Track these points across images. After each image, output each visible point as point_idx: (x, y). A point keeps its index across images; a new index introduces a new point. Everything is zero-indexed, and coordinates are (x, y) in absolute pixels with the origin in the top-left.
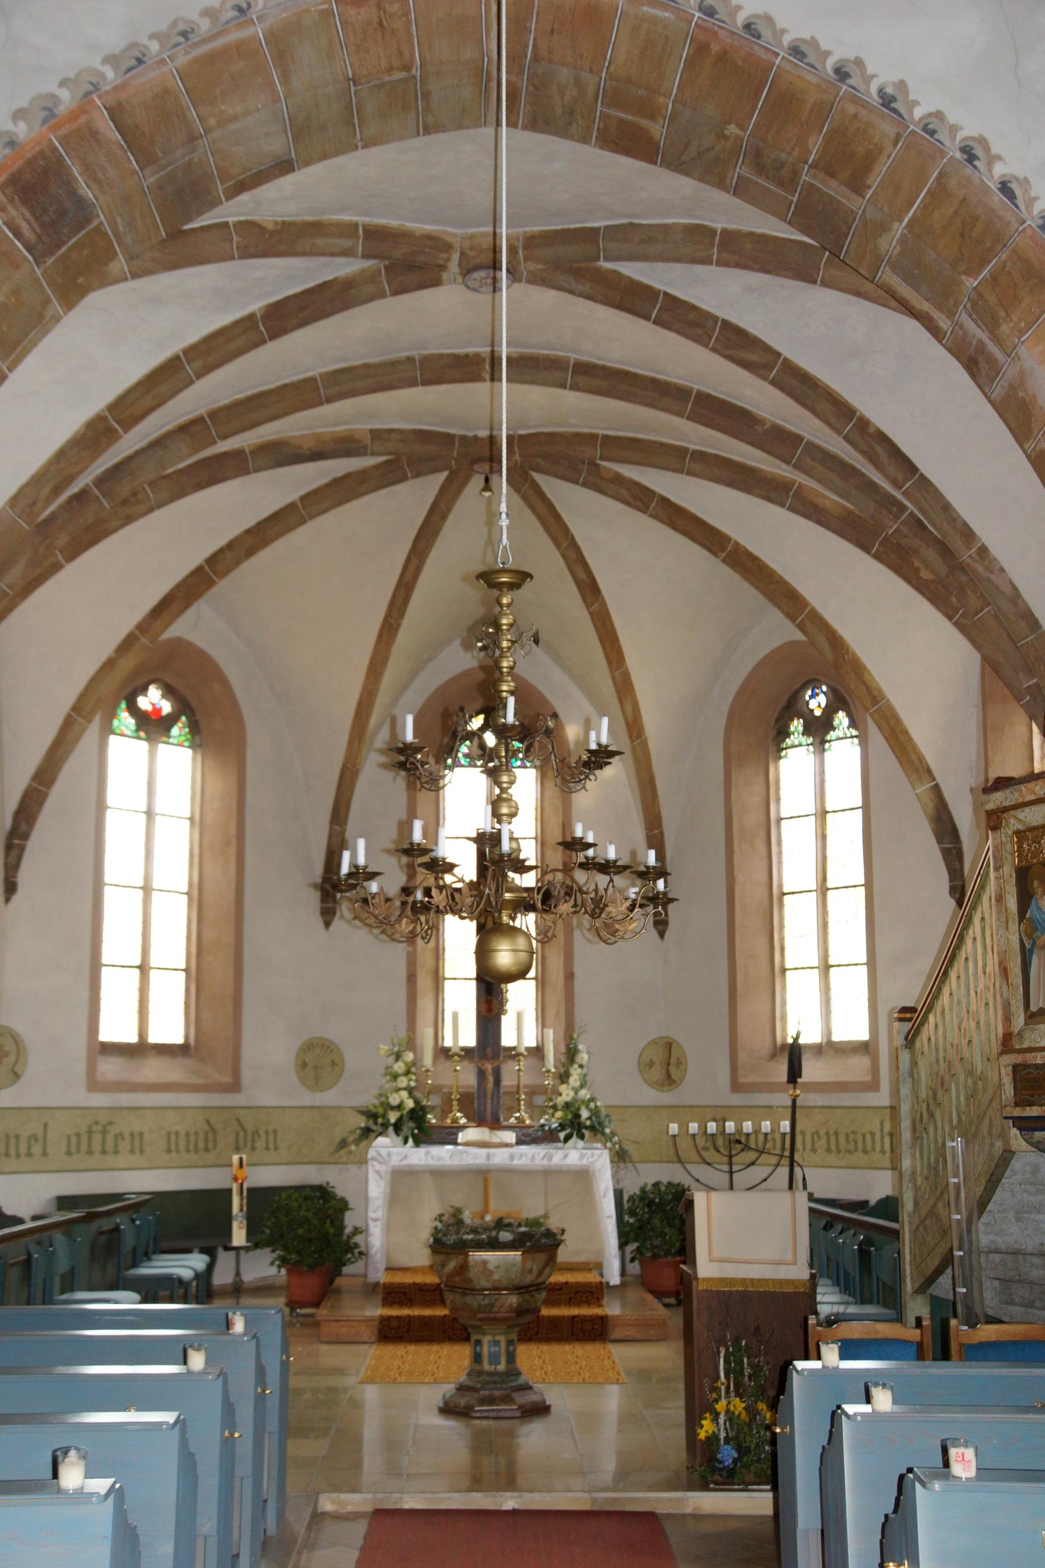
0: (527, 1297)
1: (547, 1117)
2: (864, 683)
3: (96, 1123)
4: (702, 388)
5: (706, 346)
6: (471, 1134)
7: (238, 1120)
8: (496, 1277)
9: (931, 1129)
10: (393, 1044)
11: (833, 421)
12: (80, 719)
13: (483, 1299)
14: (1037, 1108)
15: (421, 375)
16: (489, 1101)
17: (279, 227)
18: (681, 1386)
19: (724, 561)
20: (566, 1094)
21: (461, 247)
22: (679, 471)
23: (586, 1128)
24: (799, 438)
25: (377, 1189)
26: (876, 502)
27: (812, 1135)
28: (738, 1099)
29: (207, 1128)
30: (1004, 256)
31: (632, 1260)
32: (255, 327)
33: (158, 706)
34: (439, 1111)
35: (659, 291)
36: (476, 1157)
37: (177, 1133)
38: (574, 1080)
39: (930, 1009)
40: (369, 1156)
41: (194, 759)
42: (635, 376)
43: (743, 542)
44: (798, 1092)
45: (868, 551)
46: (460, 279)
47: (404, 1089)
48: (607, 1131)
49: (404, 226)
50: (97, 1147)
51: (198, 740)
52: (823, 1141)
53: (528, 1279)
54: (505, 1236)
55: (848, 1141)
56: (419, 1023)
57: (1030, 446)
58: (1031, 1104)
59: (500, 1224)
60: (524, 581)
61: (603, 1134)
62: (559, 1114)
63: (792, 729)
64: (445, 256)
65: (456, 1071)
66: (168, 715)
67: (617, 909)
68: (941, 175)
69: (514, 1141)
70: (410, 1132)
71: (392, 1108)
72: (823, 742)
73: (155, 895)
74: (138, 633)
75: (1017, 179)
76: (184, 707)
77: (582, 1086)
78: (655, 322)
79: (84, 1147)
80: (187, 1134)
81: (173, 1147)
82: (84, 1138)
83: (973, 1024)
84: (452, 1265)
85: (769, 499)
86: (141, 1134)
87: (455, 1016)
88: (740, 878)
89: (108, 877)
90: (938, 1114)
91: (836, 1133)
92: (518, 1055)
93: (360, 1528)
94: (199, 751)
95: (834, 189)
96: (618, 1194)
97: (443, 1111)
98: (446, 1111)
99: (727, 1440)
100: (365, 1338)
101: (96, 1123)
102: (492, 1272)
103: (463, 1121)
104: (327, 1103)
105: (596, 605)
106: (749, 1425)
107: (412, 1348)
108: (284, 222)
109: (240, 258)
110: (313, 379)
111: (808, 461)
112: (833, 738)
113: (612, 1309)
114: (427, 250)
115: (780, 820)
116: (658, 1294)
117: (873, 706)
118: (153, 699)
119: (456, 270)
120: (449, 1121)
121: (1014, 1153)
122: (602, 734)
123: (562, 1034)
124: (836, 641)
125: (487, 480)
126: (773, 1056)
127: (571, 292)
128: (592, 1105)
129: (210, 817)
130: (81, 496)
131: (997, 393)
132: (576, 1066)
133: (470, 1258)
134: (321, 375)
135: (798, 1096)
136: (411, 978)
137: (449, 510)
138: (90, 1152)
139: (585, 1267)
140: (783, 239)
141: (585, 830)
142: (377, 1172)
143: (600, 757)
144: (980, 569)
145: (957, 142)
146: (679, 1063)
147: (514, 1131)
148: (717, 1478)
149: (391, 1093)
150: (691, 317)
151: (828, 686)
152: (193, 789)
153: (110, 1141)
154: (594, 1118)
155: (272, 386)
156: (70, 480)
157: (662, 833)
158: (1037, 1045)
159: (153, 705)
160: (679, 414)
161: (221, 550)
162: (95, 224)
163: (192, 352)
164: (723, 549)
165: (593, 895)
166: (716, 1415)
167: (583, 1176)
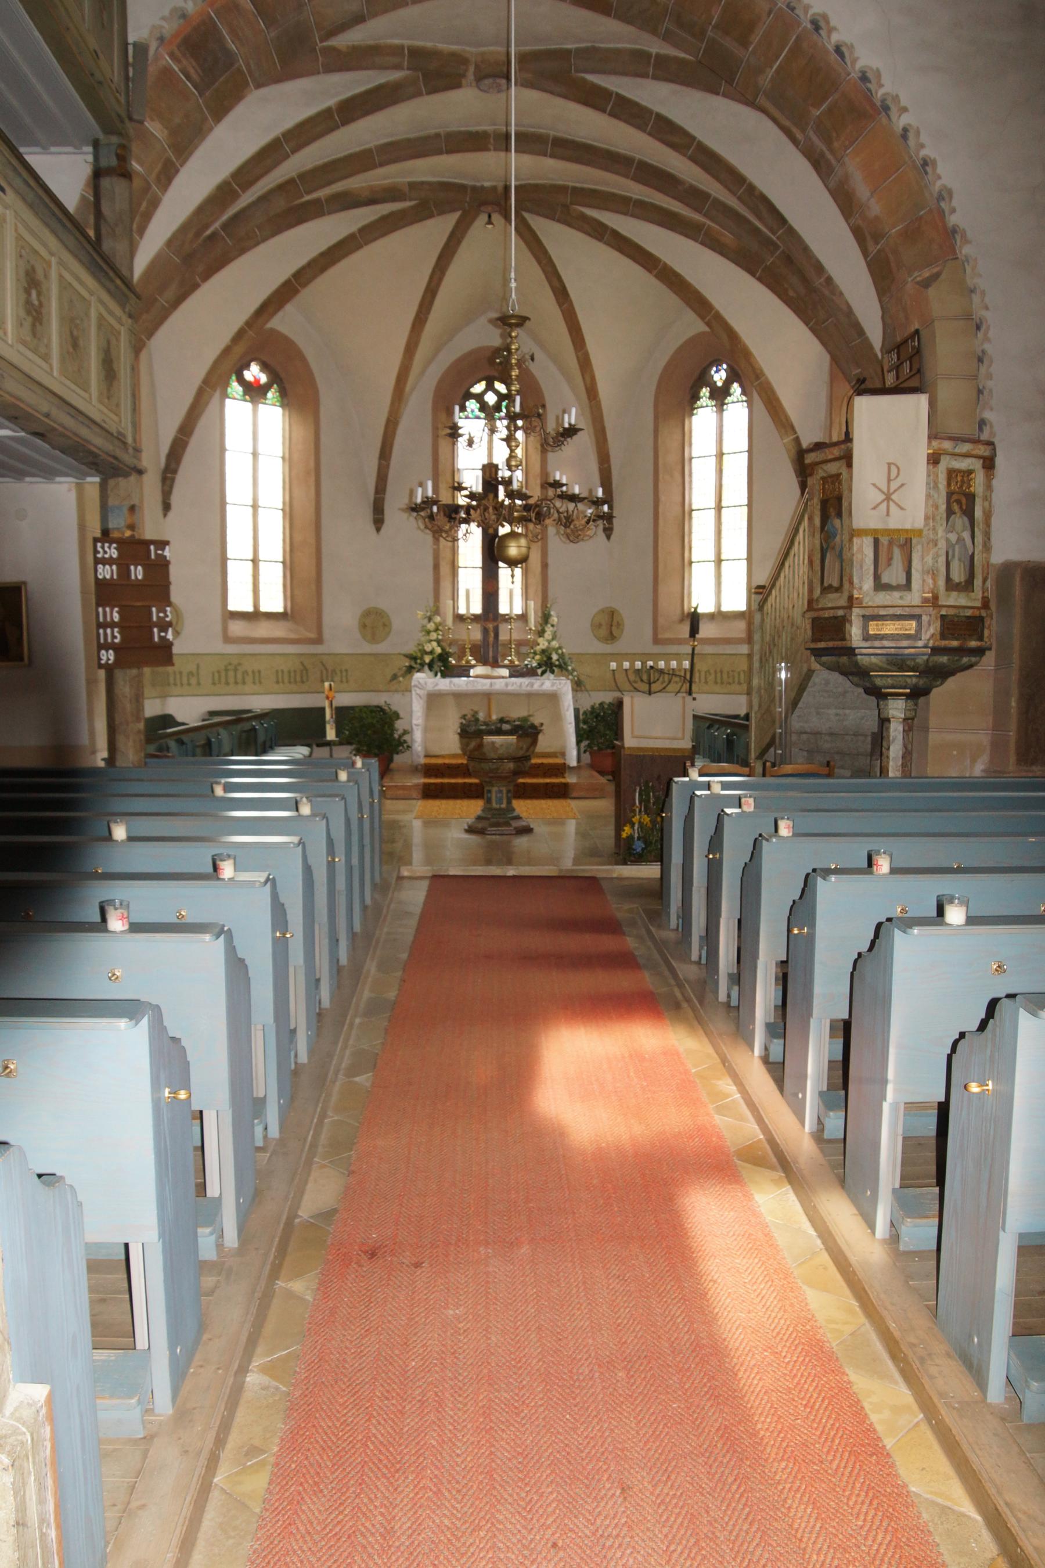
2: (751, 365)
4: (642, 158)
5: (644, 131)
6: (479, 670)
7: (322, 663)
8: (500, 751)
9: (771, 660)
15: (446, 146)
16: (491, 650)
18: (613, 820)
19: (656, 276)
20: (543, 644)
22: (625, 214)
23: (556, 666)
29: (302, 668)
30: (836, 96)
31: (585, 752)
34: (456, 656)
37: (283, 671)
38: (548, 635)
39: (773, 585)
40: (413, 684)
41: (284, 415)
43: (668, 262)
44: (696, 643)
46: (474, 84)
48: (570, 668)
50: (231, 680)
51: (286, 401)
53: (521, 753)
54: (506, 727)
55: (728, 677)
56: (442, 597)
57: (852, 221)
58: (821, 641)
59: (502, 721)
60: (525, 321)
61: (567, 670)
62: (538, 657)
63: (702, 394)
67: (580, 523)
68: (798, 38)
72: (723, 404)
75: (846, 44)
76: (276, 378)
77: (553, 639)
79: (223, 680)
80: (289, 672)
81: (280, 680)
82: (223, 674)
83: (796, 595)
84: (473, 744)
85: (687, 236)
86: (259, 672)
89: (229, 499)
90: (775, 651)
91: (721, 672)
92: (511, 618)
93: (425, 884)
95: (729, 43)
96: (577, 711)
97: (459, 657)
98: (461, 655)
99: (639, 838)
100: (414, 796)
101: (230, 664)
102: (497, 748)
105: (565, 305)
106: (652, 829)
107: (444, 802)
110: (370, 150)
113: (571, 779)
116: (602, 773)
118: (254, 373)
119: (472, 78)
120: (464, 662)
121: (814, 671)
122: (571, 418)
123: (539, 604)
124: (732, 335)
125: (490, 216)
126: (682, 620)
127: (552, 93)
130: (214, 236)
131: (832, 184)
132: (549, 626)
133: (485, 741)
134: (376, 147)
136: (436, 567)
137: (463, 238)
138: (227, 683)
139: (554, 755)
141: (561, 477)
143: (571, 431)
144: (827, 292)
145: (809, 16)
146: (619, 625)
148: (633, 859)
152: (284, 437)
153: (239, 676)
155: (341, 155)
156: (207, 226)
157: (609, 467)
159: (255, 377)
162: (236, 65)
163: (288, 135)
165: (565, 514)
166: (633, 825)
167: (553, 698)
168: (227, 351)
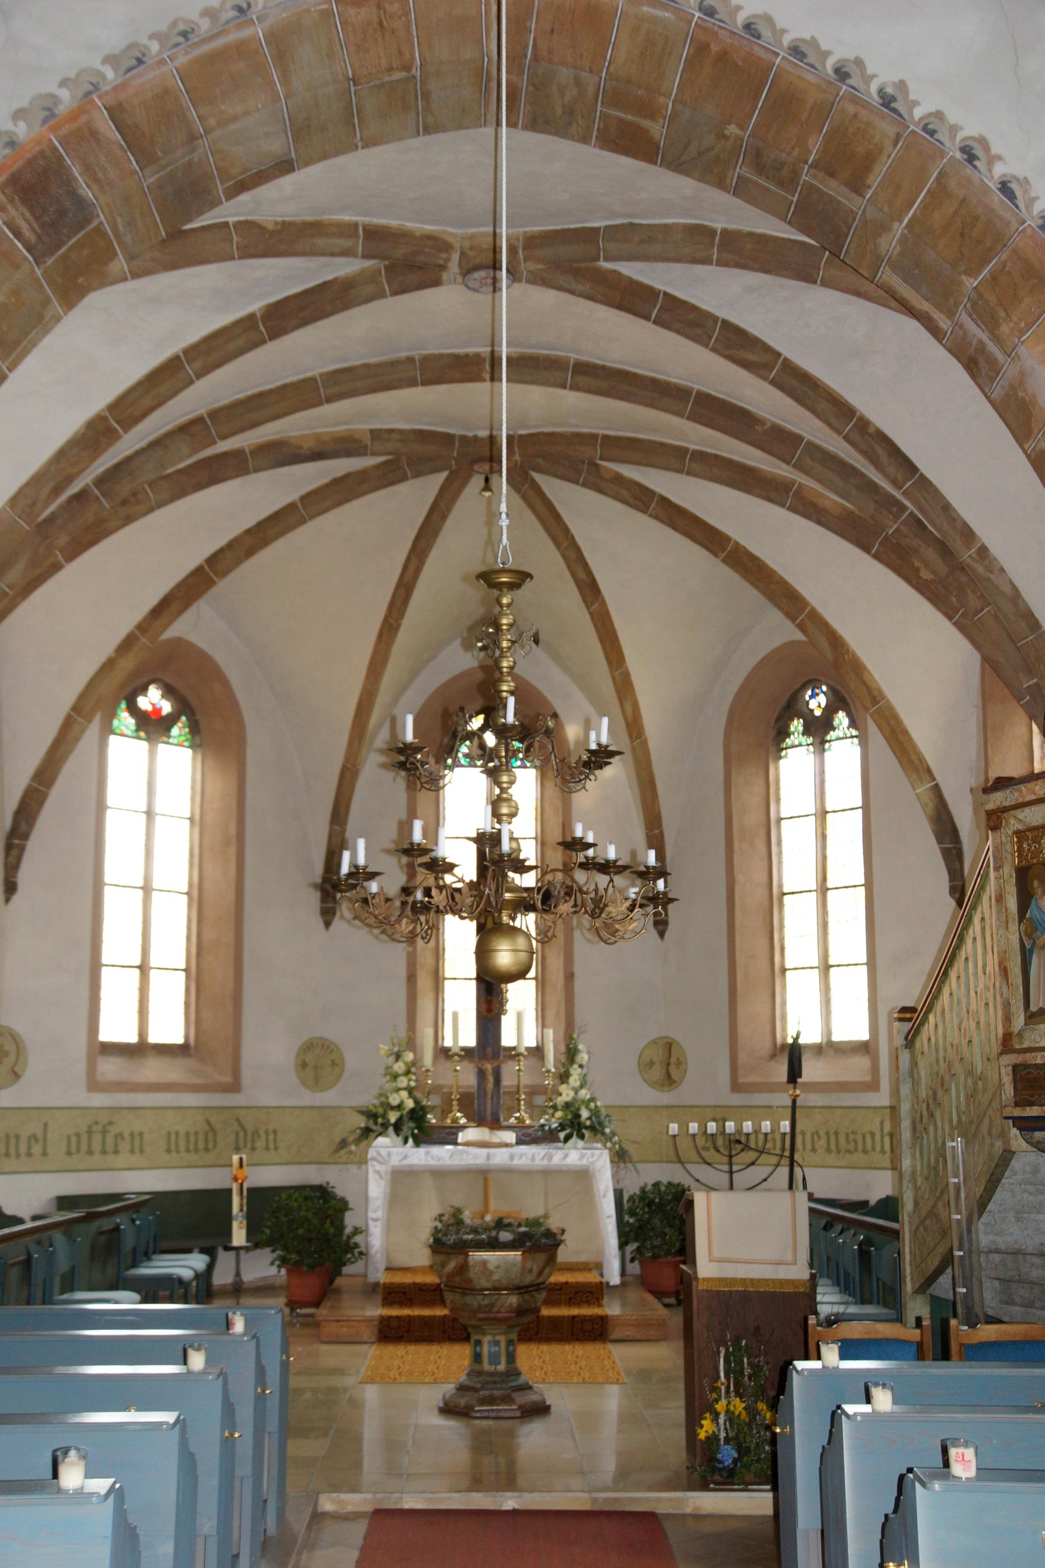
0: (527, 1297)
1: (547, 1117)
2: (864, 683)
3: (96, 1123)
4: (702, 388)
5: (706, 346)
6: (471, 1134)
7: (238, 1120)
8: (496, 1277)
9: (931, 1129)
10: (393, 1044)
11: (833, 421)
12: (80, 719)
13: (483, 1299)
14: (1037, 1108)
15: (421, 375)
16: (489, 1101)
17: (279, 227)
18: (681, 1386)
19: (724, 561)
20: (566, 1094)
21: (461, 247)
22: (679, 471)
23: (586, 1128)
24: (799, 438)
25: (377, 1189)
26: (876, 502)
27: (812, 1135)
28: (738, 1099)
29: (207, 1128)
30: (1004, 256)
31: (632, 1260)
32: (255, 327)
33: (158, 706)
34: (439, 1111)
35: (659, 291)
36: (476, 1157)
37: (177, 1133)
38: (574, 1080)
39: (930, 1009)
40: (369, 1156)
41: (194, 759)
42: (635, 376)
43: (743, 542)
44: (798, 1092)
45: (868, 551)
46: (460, 279)
47: (404, 1089)
48: (607, 1131)
49: (404, 226)
50: (97, 1147)
51: (198, 740)
52: (823, 1141)
53: (528, 1279)
54: (505, 1236)
55: (848, 1141)
56: (419, 1023)
57: (1030, 446)
58: (1031, 1104)
59: (500, 1224)
60: (524, 581)
61: (603, 1134)
62: (559, 1114)
63: (792, 729)
64: (445, 256)
65: (456, 1071)
66: (168, 715)
67: (617, 909)
68: (941, 175)
69: (514, 1141)
70: (410, 1132)
71: (392, 1108)
72: (823, 742)
73: (155, 895)
74: (138, 633)
75: (1017, 179)
76: (184, 707)
77: (582, 1086)
78: (655, 322)
79: (84, 1147)
80: (187, 1134)
81: (173, 1147)
82: (84, 1138)
83: (973, 1024)
84: (452, 1265)
85: (769, 499)
86: (141, 1134)
87: (455, 1016)
88: (740, 878)
89: (108, 877)
90: (938, 1114)
91: (836, 1133)
92: (518, 1055)
93: (360, 1528)
94: (199, 751)
95: (834, 189)
96: (618, 1194)
97: (443, 1111)
98: (446, 1111)
99: (727, 1440)
100: (365, 1338)
101: (96, 1123)
102: (492, 1272)
103: (463, 1121)
104: (327, 1103)
106: (749, 1425)
107: (412, 1348)
108: (284, 222)
109: (240, 258)
110: (313, 379)
111: (808, 461)
112: (833, 738)
113: (612, 1309)
114: (427, 250)
115: (780, 820)
116: (658, 1294)
117: (873, 706)
118: (153, 699)
119: (456, 270)
120: (449, 1121)
121: (1014, 1153)
122: (602, 734)
123: (562, 1034)
124: (836, 641)
125: (487, 480)
126: (773, 1056)
127: (571, 292)
128: (592, 1105)
129: (210, 817)
130: (81, 496)
131: (997, 393)
132: (576, 1066)
133: (470, 1258)
134: (321, 375)
135: (798, 1096)
136: (411, 978)
137: (449, 510)
138: (90, 1152)
139: (585, 1267)
140: (783, 239)
141: (585, 830)
142: (377, 1172)
143: (600, 757)
144: (980, 569)
145: (957, 142)
146: (679, 1063)
147: (514, 1131)
148: (717, 1478)
149: (391, 1093)
150: (691, 317)
151: (828, 686)
152: (193, 789)
153: (110, 1141)
154: (594, 1118)
155: (272, 386)
156: (70, 480)
157: (662, 833)
158: (1037, 1045)
159: (153, 705)
160: (679, 414)
161: (221, 550)
162: (95, 224)
163: (192, 352)
164: (723, 549)
165: (593, 895)
166: (716, 1415)
167: (583, 1176)
168: (109, 665)
